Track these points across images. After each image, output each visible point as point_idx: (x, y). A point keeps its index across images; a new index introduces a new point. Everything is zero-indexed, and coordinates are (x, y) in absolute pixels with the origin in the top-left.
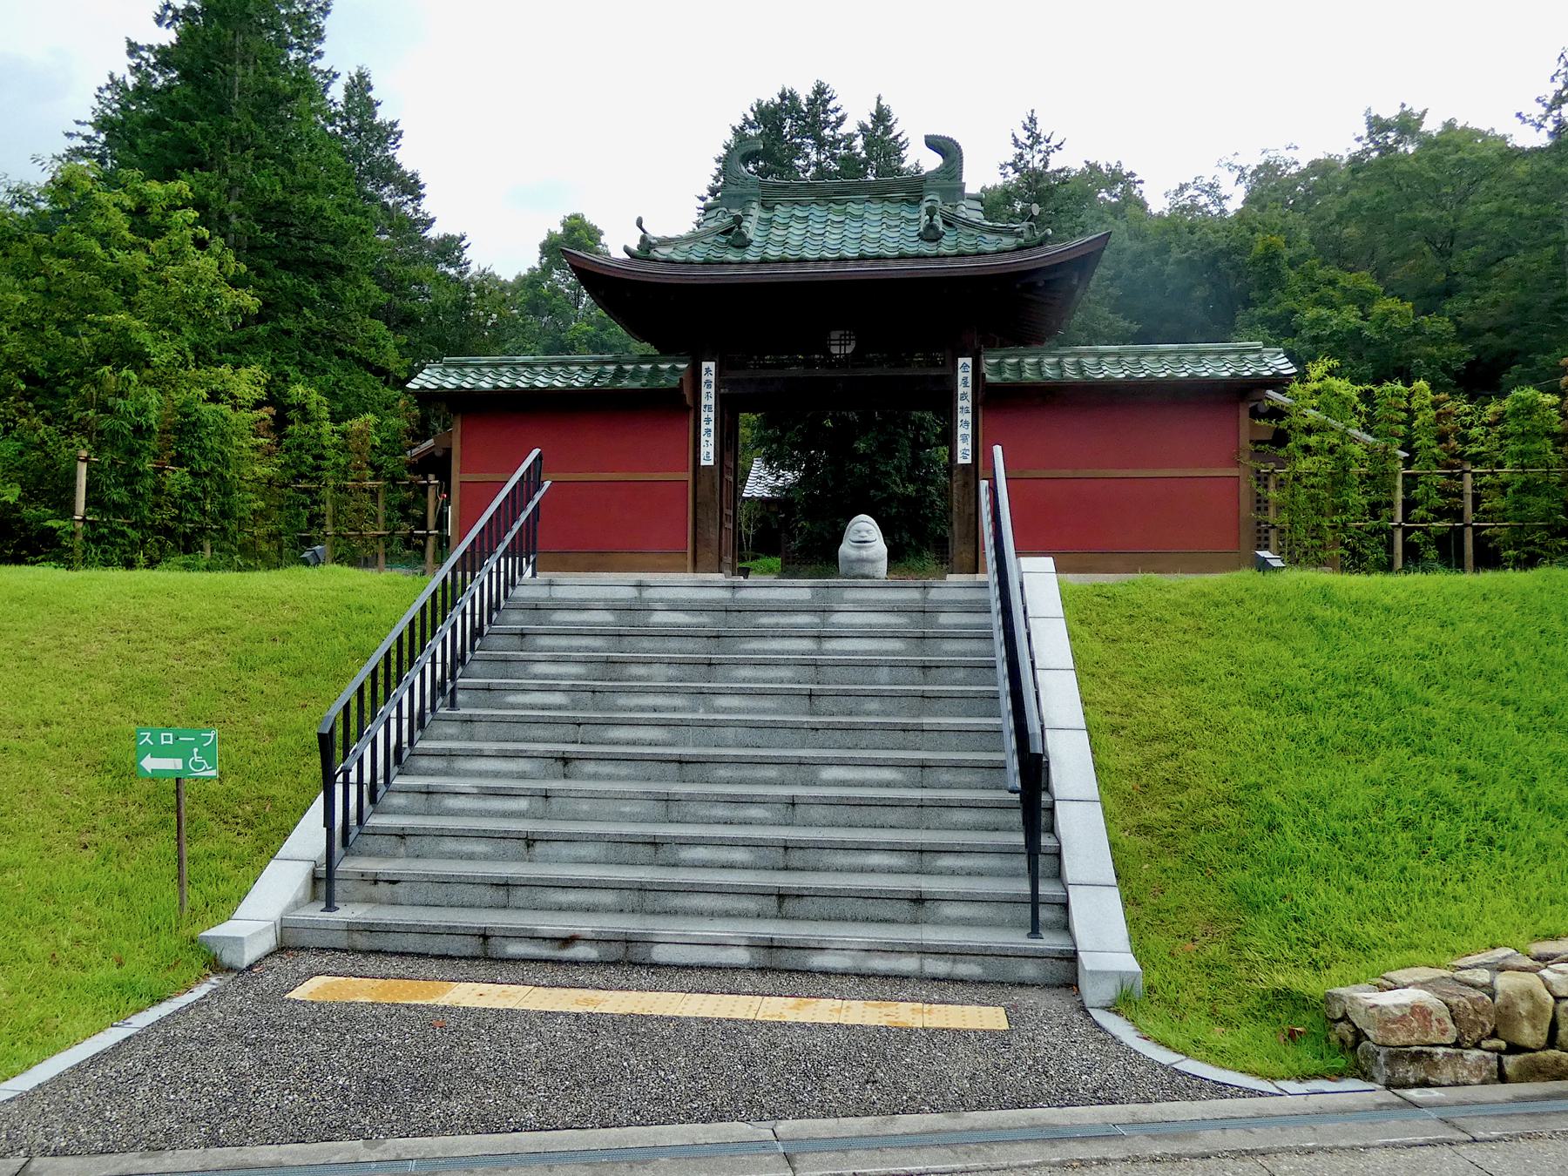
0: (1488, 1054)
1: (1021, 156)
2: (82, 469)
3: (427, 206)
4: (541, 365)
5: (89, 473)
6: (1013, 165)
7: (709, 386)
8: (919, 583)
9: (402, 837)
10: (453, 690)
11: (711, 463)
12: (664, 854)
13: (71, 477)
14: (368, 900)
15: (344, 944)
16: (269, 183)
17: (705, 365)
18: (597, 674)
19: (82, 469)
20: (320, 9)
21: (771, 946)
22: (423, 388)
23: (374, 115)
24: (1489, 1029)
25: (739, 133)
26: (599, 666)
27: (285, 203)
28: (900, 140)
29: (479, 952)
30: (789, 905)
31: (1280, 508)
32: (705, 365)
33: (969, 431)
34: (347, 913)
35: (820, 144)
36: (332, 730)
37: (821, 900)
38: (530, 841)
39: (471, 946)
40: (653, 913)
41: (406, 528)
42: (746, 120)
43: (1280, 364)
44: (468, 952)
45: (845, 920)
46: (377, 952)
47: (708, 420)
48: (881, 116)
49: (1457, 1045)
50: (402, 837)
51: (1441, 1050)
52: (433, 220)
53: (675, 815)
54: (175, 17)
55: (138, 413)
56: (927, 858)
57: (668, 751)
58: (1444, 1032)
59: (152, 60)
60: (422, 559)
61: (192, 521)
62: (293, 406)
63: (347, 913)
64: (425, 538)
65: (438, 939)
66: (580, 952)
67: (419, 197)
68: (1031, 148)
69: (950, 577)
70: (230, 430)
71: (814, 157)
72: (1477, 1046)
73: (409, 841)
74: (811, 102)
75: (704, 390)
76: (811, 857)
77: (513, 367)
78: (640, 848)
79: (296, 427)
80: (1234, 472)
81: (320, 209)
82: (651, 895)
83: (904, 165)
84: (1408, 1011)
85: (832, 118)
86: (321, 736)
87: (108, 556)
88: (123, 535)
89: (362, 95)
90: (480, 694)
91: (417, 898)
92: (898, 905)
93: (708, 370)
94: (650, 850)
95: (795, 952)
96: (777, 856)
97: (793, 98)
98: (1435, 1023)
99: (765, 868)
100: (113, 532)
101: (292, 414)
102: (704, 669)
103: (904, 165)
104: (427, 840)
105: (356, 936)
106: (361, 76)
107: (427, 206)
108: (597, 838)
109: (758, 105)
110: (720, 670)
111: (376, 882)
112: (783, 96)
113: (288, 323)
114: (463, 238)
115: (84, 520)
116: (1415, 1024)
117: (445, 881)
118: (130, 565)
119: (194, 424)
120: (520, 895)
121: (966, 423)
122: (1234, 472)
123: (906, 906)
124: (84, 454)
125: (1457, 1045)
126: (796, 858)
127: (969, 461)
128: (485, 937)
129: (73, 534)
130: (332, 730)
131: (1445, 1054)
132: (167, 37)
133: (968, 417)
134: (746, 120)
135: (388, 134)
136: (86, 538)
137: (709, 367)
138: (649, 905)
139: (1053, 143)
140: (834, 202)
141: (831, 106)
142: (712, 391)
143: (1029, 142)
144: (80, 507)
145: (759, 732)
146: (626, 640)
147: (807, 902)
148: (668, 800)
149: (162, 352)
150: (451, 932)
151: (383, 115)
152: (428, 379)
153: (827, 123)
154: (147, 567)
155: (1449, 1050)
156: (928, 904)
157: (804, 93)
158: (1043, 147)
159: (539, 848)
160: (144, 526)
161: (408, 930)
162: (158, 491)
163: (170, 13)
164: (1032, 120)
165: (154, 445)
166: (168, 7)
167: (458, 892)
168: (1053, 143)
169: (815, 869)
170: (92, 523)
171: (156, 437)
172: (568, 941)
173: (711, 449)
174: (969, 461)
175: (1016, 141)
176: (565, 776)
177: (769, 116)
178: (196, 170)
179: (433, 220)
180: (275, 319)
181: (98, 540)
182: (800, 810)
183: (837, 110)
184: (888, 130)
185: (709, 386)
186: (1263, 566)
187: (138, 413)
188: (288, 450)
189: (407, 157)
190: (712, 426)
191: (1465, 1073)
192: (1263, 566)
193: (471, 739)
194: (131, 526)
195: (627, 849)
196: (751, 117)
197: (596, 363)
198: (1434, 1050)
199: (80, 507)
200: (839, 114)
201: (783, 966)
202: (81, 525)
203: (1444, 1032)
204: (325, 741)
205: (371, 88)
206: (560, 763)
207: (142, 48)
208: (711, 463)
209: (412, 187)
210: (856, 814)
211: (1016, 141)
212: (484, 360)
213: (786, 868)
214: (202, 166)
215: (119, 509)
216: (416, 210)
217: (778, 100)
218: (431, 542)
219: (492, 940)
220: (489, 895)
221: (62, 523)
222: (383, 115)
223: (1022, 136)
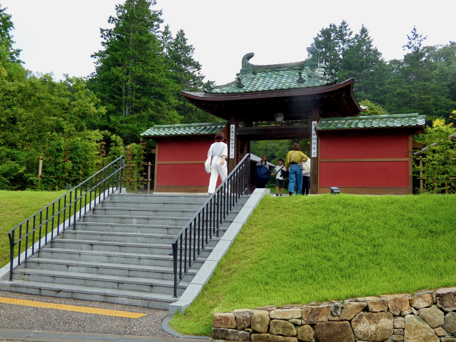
0: (246, 333)
1: (411, 43)
2: (41, 162)
3: (203, 72)
4: (182, 127)
5: (43, 163)
6: (407, 46)
7: (233, 133)
8: (144, 195)
9: (39, 263)
10: (218, 231)
11: (233, 157)
12: (100, 271)
13: (38, 164)
14: (23, 279)
15: (9, 290)
16: (139, 71)
17: (232, 126)
18: (119, 221)
19: (41, 162)
20: (159, 13)
21: (105, 295)
22: (145, 135)
23: (186, 43)
24: (247, 325)
25: (316, 39)
26: (119, 219)
27: (143, 76)
28: (371, 39)
29: (38, 293)
30: (120, 285)
31: (424, 172)
32: (232, 126)
33: (316, 146)
34: (15, 282)
35: (344, 42)
36: (13, 232)
37: (128, 285)
38: (68, 266)
39: (37, 292)
40: (88, 286)
41: (142, 178)
42: (318, 35)
43: (421, 122)
44: (36, 293)
45: (134, 290)
46: (17, 292)
47: (232, 143)
48: (364, 31)
49: (236, 328)
50: (39, 263)
51: (230, 330)
52: (205, 76)
53: (110, 261)
54: (113, 20)
55: (58, 145)
56: (164, 275)
57: (147, 245)
58: (232, 325)
59: (106, 34)
60: (146, 188)
61: (74, 177)
62: (112, 141)
63: (15, 282)
64: (147, 182)
65: (30, 289)
66: (61, 294)
67: (199, 69)
68: (414, 39)
69: (155, 193)
70: (88, 149)
71: (342, 46)
72: (243, 329)
73: (40, 264)
74: (341, 27)
75: (231, 134)
76: (135, 273)
77: (164, 129)
78: (94, 269)
79: (113, 148)
80: (406, 159)
81: (154, 77)
82: (87, 281)
83: (371, 48)
84: (223, 318)
85: (348, 32)
86: (173, 245)
87: (46, 187)
88: (52, 181)
89: (182, 37)
90: (84, 226)
91: (34, 279)
92: (147, 287)
93: (232, 127)
94: (96, 269)
95: (111, 297)
96: (126, 272)
97: (334, 26)
98: (230, 322)
99: (124, 276)
100: (48, 180)
101: (112, 144)
102: (146, 220)
103: (371, 48)
104: (44, 265)
105: (12, 288)
106: (181, 31)
107: (203, 72)
108: (84, 266)
109: (323, 29)
110: (150, 221)
111: (25, 274)
112: (331, 26)
113: (143, 114)
114: (214, 82)
115: (41, 177)
116: (224, 322)
117: (40, 275)
118: (54, 189)
119: (76, 148)
120: (57, 279)
121: (315, 143)
122: (406, 159)
123: (149, 287)
124: (41, 157)
125: (236, 328)
126: (131, 273)
127: (316, 156)
128: (72, 292)
129: (38, 181)
130: (13, 232)
131: (232, 331)
132: (112, 26)
133: (316, 141)
134: (318, 35)
135: (188, 49)
136: (41, 182)
137: (233, 126)
138: (87, 284)
139: (422, 38)
140: (276, 71)
141: (347, 28)
142: (234, 134)
143: (414, 37)
144: (40, 173)
145: (147, 238)
146: (132, 212)
147: (125, 285)
148: (109, 256)
149: (68, 127)
150: (33, 288)
151: (188, 44)
152: (150, 132)
153: (346, 34)
154: (59, 190)
155: (233, 330)
156: (154, 287)
157: (338, 25)
158: (419, 39)
159: (70, 268)
160: (59, 178)
161: (23, 287)
162: (63, 168)
163: (111, 19)
164: (415, 29)
165: (63, 154)
166: (110, 17)
167: (43, 278)
168: (422, 38)
169: (136, 277)
170: (43, 177)
171: (63, 152)
172: (59, 291)
173: (233, 153)
174: (316, 156)
175: (409, 37)
176: (92, 249)
177: (326, 33)
178: (117, 67)
179: (205, 76)
180: (140, 112)
181: (44, 182)
182: (142, 260)
183: (350, 29)
184: (366, 35)
185: (233, 133)
186: (332, 191)
187: (58, 145)
188: (110, 155)
189: (195, 56)
190: (233, 145)
191: (238, 337)
192: (332, 191)
193: (75, 239)
194: (55, 178)
195: (91, 269)
196: (320, 34)
197: (198, 126)
198: (228, 330)
199: (40, 173)
200: (350, 31)
201: (109, 301)
202: (40, 178)
203: (232, 325)
204: (175, 246)
205: (184, 35)
206: (90, 246)
207: (104, 30)
208: (233, 157)
209: (197, 66)
210: (156, 262)
211: (409, 37)
212: (166, 126)
213: (129, 276)
214: (119, 65)
215: (52, 173)
216: (199, 73)
217: (329, 27)
218: (149, 183)
219: (42, 290)
220: (51, 279)
221: (35, 178)
222: (188, 44)
223: (411, 35)
